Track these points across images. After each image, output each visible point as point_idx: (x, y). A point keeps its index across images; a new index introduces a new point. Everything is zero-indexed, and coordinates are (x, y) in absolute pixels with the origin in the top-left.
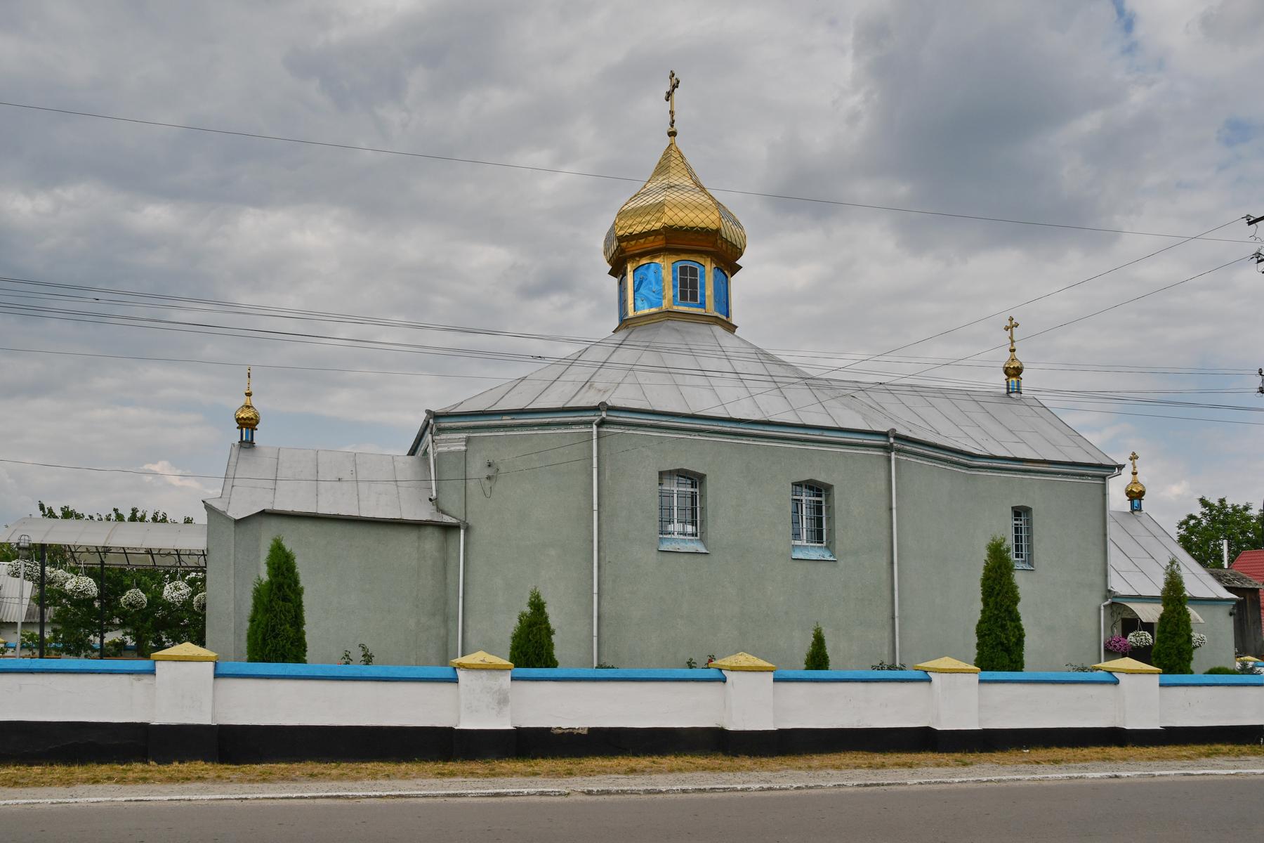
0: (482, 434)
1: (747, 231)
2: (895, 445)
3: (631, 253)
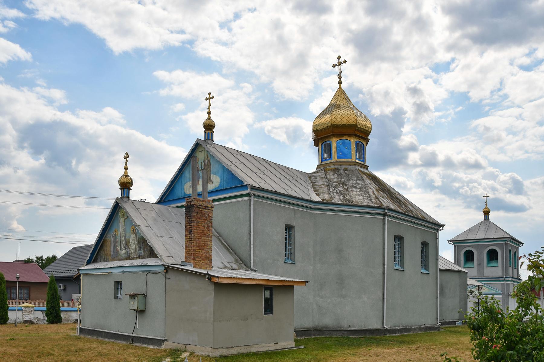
2: (387, 213)
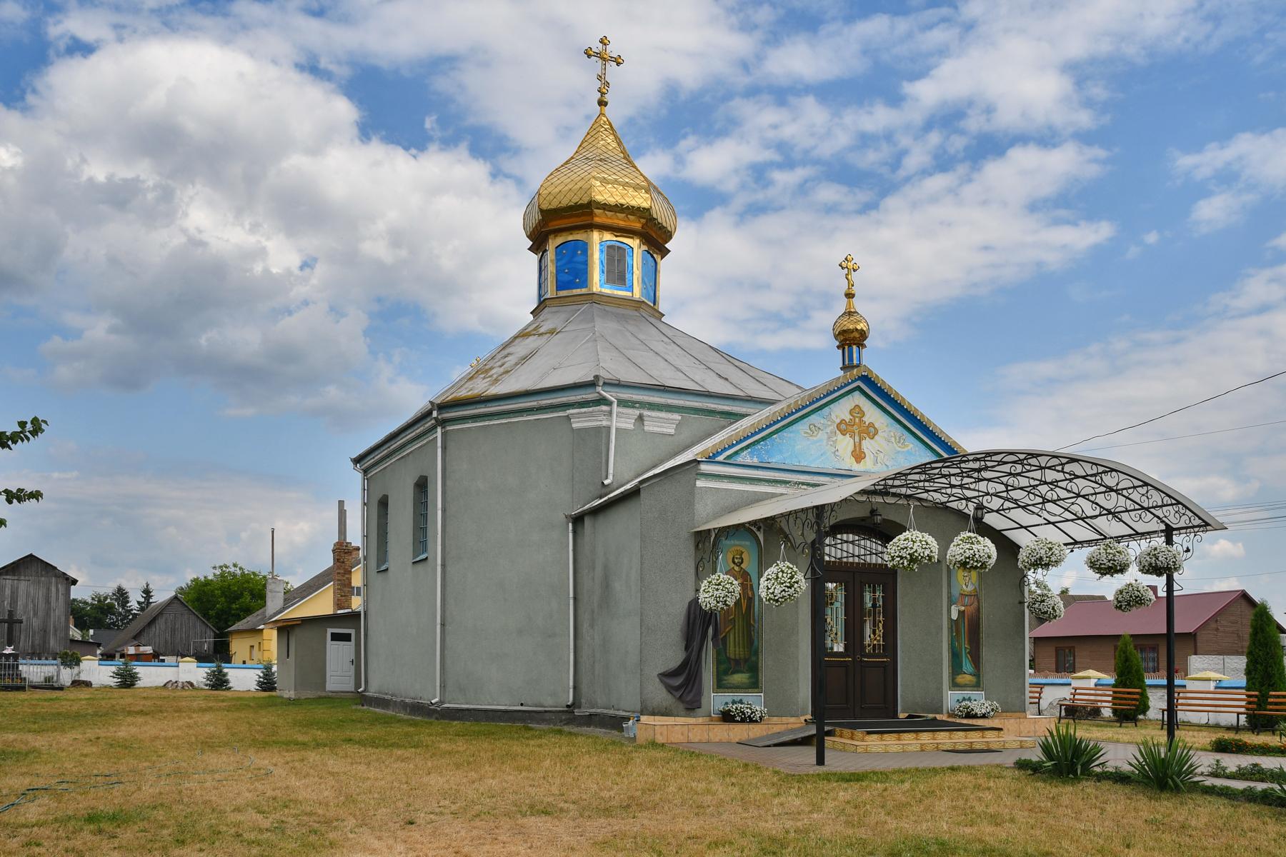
0: (492, 423)
3: (554, 228)
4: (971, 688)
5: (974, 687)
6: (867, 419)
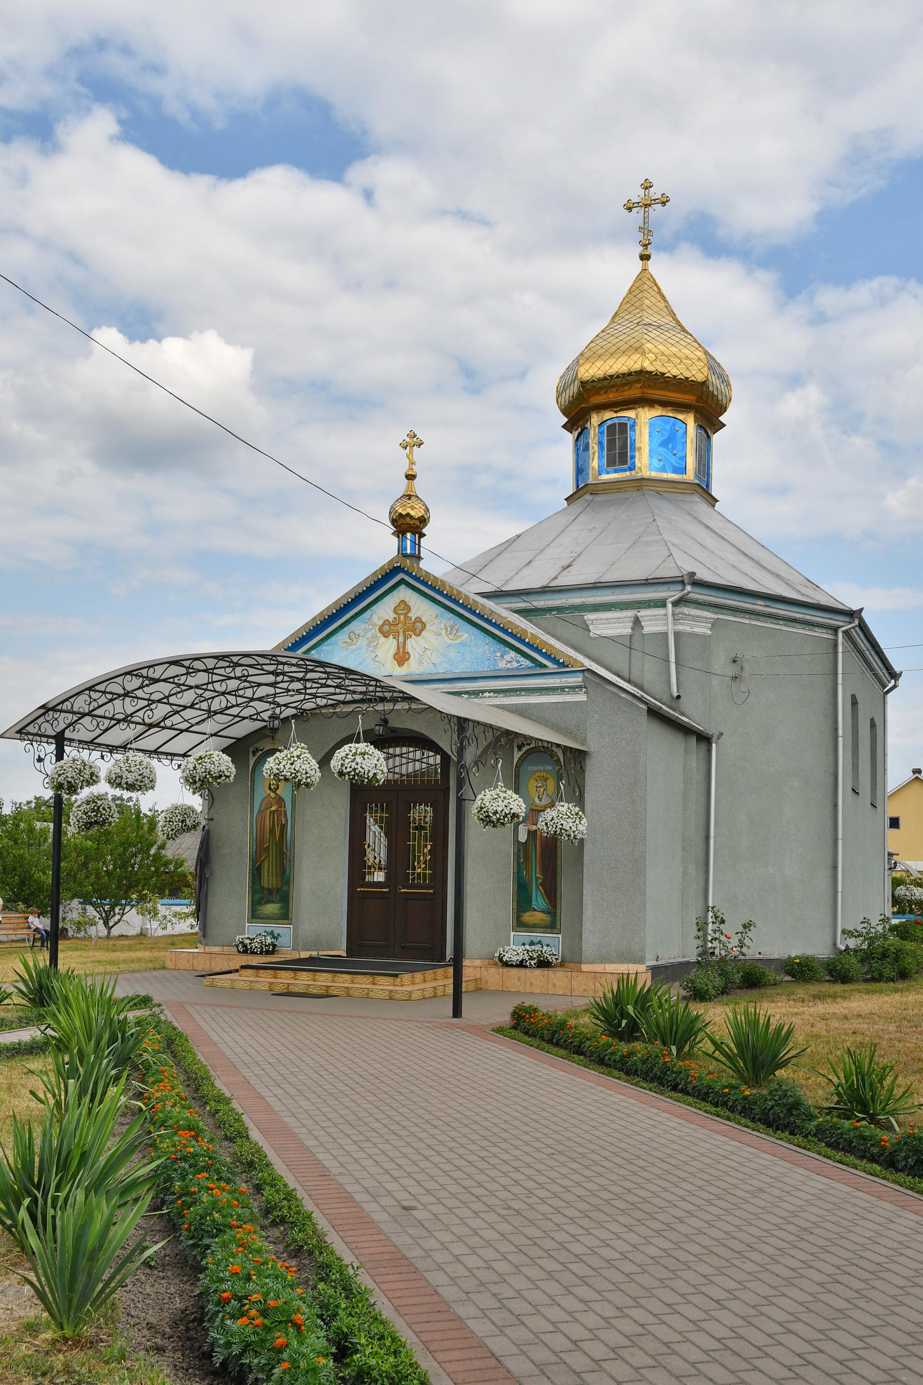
0: (726, 617)
1: (735, 394)
4: (543, 930)
5: (546, 927)
6: (413, 615)
